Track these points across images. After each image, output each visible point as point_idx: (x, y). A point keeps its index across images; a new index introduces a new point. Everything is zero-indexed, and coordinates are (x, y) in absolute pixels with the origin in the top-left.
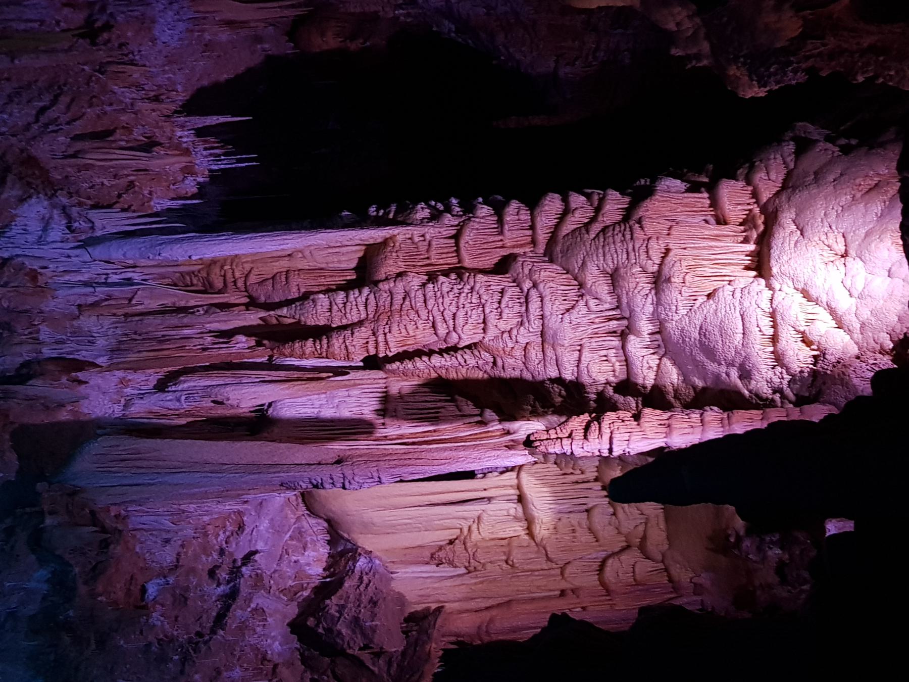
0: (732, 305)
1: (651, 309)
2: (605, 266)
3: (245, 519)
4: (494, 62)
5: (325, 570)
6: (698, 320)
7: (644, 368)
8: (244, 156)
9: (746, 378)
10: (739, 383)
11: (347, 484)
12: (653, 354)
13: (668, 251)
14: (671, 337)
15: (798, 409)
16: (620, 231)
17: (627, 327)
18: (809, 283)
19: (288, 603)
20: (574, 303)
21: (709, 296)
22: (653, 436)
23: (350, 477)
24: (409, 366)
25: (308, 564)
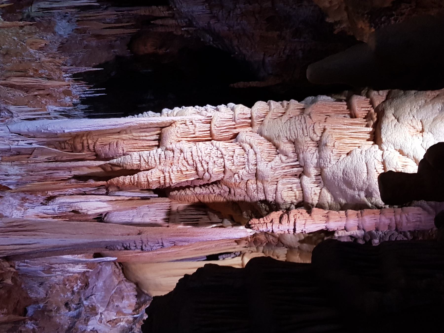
0: (360, 158)
1: (316, 161)
2: (291, 138)
3: (89, 280)
4: (232, 56)
5: (133, 311)
6: (342, 166)
7: (312, 194)
8: (98, 89)
9: (369, 197)
10: (366, 200)
11: (144, 247)
12: (317, 186)
13: (325, 129)
14: (327, 176)
15: (400, 209)
16: (299, 119)
17: (303, 172)
18: (403, 146)
19: (112, 328)
20: (274, 158)
21: (348, 154)
22: (319, 222)
23: (145, 243)
24: (183, 193)
25: (125, 308)
